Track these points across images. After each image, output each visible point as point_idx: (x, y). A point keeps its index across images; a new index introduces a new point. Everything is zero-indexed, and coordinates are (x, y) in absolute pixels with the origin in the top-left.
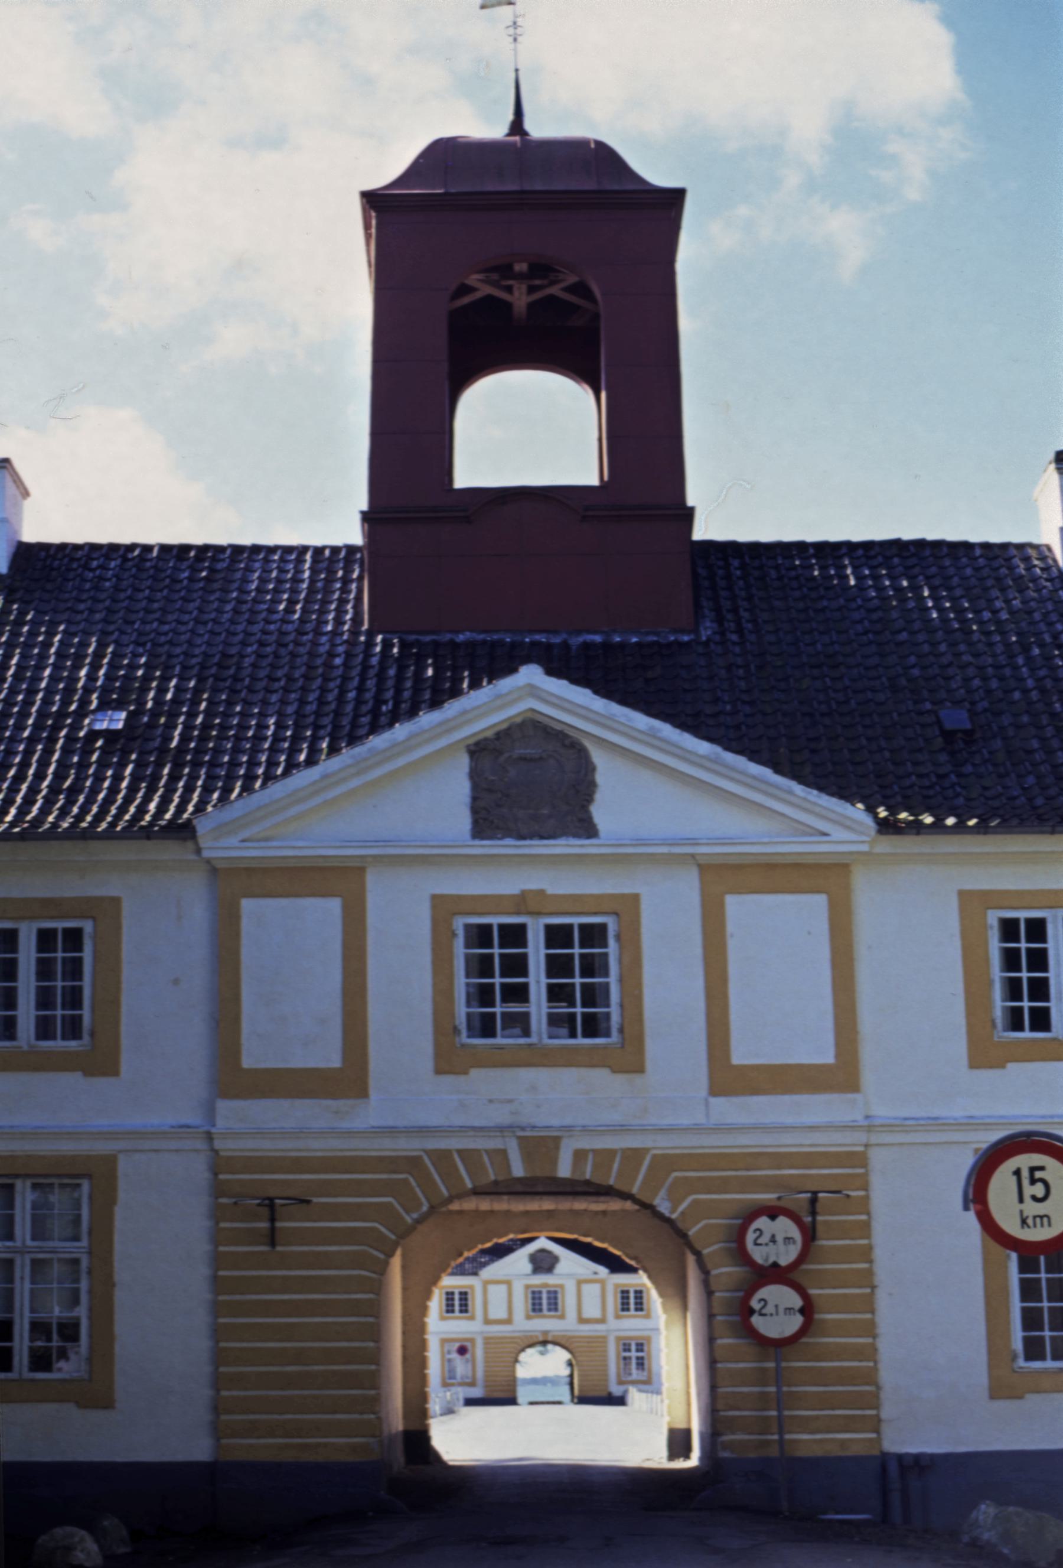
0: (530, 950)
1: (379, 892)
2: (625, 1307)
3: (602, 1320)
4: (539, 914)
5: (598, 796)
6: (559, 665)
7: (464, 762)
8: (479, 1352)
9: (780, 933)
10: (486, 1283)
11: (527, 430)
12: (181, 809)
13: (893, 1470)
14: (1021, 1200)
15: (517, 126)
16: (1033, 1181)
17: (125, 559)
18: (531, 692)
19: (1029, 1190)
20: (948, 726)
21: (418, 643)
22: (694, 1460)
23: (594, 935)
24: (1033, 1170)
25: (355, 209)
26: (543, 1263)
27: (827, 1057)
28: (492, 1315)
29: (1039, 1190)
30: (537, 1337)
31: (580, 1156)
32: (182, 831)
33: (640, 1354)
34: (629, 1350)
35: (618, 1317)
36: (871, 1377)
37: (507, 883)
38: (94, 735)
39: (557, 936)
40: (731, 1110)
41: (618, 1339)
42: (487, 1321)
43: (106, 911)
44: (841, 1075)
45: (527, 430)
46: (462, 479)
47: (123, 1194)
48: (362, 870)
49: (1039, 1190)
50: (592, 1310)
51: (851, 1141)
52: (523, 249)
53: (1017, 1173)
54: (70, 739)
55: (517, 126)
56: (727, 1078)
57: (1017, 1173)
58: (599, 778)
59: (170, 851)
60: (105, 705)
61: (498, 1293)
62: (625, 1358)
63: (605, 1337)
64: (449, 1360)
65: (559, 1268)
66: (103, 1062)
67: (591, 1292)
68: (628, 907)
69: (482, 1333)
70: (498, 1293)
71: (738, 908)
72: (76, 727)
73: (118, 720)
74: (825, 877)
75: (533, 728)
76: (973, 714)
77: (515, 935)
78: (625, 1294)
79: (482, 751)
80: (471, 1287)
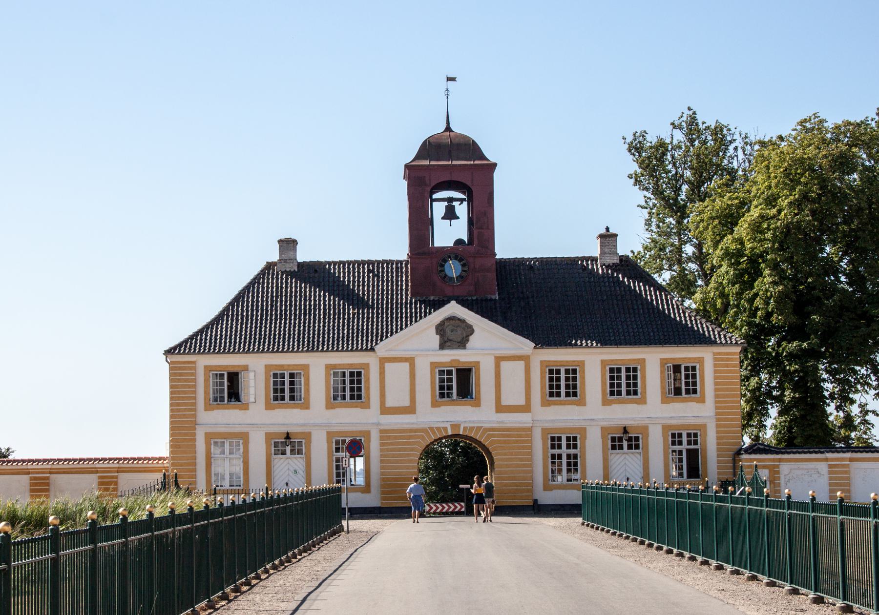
3: (526, 408)
8: (374, 446)
10: (383, 361)
15: (448, 129)
26: (453, 335)
28: (506, 401)
30: (445, 429)
33: (572, 451)
34: (560, 447)
35: (545, 404)
37: (447, 359)
40: (372, 489)
41: (545, 431)
42: (385, 410)
46: (437, 244)
50: (513, 394)
52: (450, 168)
55: (448, 129)
56: (500, 408)
59: (371, 353)
61: (397, 374)
62: (553, 456)
63: (530, 429)
64: (338, 460)
65: (473, 341)
67: (513, 372)
69: (379, 424)
70: (397, 374)
80: (366, 366)
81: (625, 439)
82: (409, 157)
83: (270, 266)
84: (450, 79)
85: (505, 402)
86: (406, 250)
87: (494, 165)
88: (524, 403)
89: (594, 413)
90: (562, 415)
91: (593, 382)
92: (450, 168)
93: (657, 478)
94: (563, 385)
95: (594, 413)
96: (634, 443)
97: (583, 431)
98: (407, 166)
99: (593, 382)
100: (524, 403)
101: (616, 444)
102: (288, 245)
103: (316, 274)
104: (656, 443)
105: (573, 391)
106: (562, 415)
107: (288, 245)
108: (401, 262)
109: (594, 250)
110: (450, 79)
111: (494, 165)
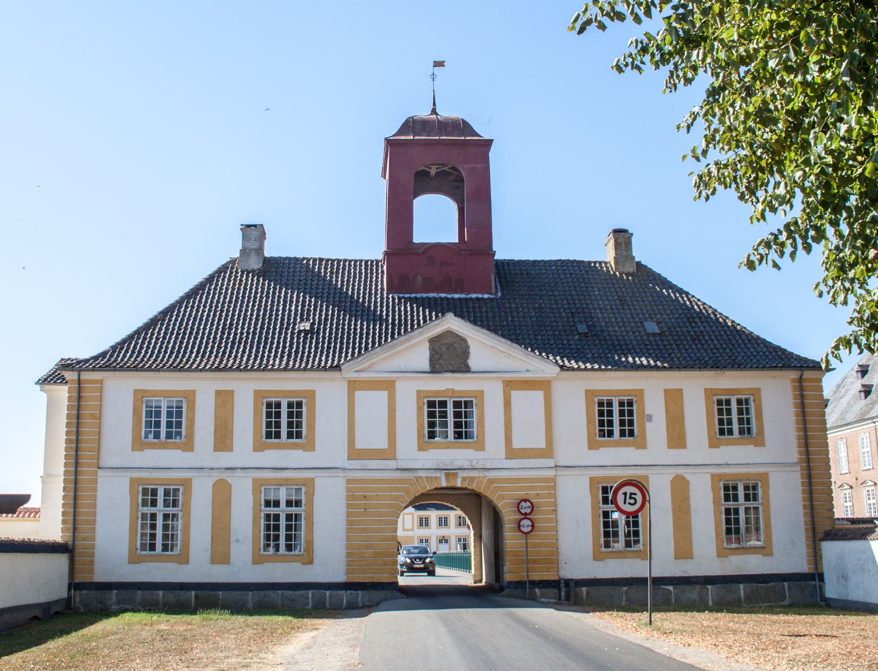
0: (448, 409)
1: (399, 386)
2: (421, 525)
3: (412, 530)
4: (452, 397)
5: (471, 356)
6: (460, 314)
7: (426, 346)
9: (529, 404)
11: (436, 220)
12: (333, 360)
13: (572, 584)
14: (625, 503)
15: (434, 111)
16: (631, 498)
17: (301, 264)
18: (452, 323)
19: (628, 500)
20: (580, 331)
21: (404, 298)
22: (483, 583)
23: (468, 404)
24: (631, 494)
25: (648, 446)
27: (543, 445)
28: (406, 527)
29: (632, 501)
31: (464, 479)
32: (338, 368)
36: (93, 553)
38: (300, 332)
39: (457, 404)
43: (311, 395)
44: (548, 452)
45: (436, 220)
46: (416, 240)
47: (317, 491)
48: (394, 381)
49: (632, 501)
51: (551, 473)
52: (438, 157)
53: (625, 494)
54: (293, 333)
57: (625, 494)
58: (471, 350)
59: (335, 374)
60: (302, 320)
66: (310, 447)
68: (480, 394)
71: (516, 395)
72: (294, 328)
73: (306, 326)
74: (544, 385)
75: (449, 333)
76: (588, 327)
77: (443, 404)
78: (421, 519)
79: (433, 342)
81: (443, 540)
82: (391, 130)
83: (233, 261)
84: (439, 64)
85: (517, 444)
86: (383, 247)
87: (489, 143)
88: (544, 446)
89: (434, 532)
90: (424, 532)
91: (434, 521)
92: (438, 157)
93: (453, 551)
94: (424, 523)
95: (434, 532)
96: (446, 541)
97: (430, 537)
98: (390, 143)
99: (434, 521)
100: (544, 446)
101: (441, 541)
102: (254, 233)
103: (280, 271)
104: (453, 541)
105: (427, 525)
106: (424, 532)
107: (254, 233)
108: (377, 262)
109: (606, 254)
110: (439, 64)
111: (489, 143)
